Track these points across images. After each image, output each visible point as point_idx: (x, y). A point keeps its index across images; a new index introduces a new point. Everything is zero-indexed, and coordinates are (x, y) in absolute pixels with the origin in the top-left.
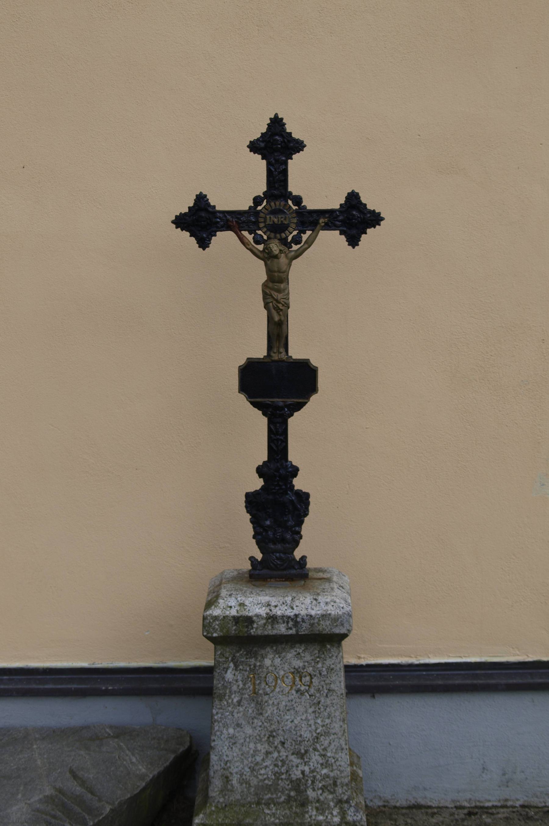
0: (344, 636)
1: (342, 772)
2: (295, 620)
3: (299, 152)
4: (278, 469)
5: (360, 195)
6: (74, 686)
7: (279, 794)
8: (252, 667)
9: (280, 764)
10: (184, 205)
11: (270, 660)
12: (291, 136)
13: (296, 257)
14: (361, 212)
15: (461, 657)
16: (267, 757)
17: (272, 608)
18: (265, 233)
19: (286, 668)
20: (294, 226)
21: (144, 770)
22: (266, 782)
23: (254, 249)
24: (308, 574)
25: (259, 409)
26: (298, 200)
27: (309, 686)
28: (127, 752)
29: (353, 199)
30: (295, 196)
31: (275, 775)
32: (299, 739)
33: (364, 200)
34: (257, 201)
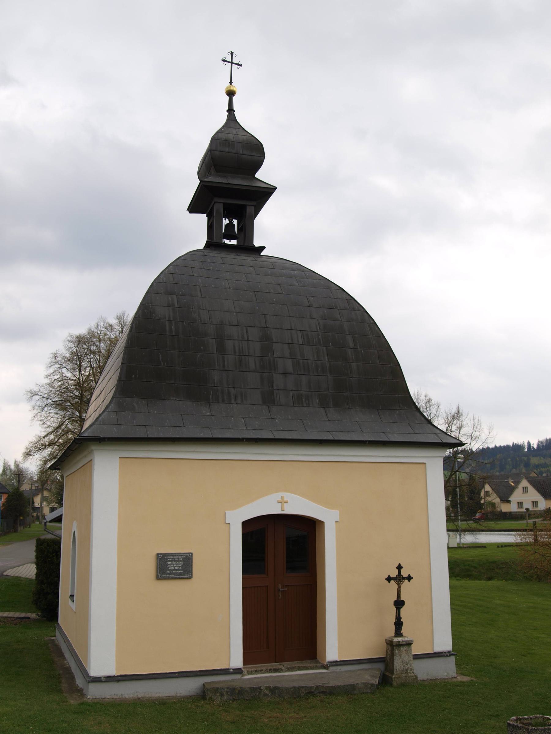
2: (406, 641)
11: (402, 649)
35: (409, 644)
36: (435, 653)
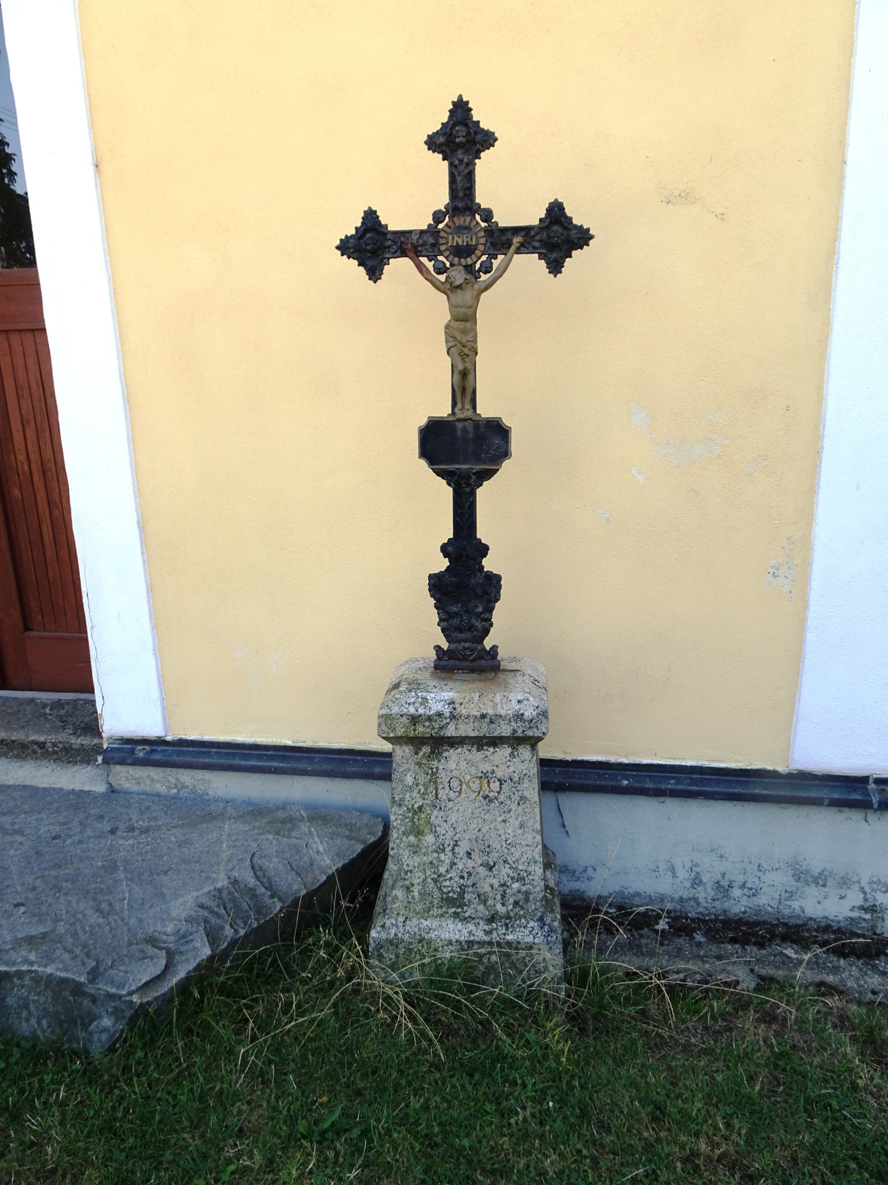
0: (540, 739)
1: (534, 887)
3: (488, 149)
4: (465, 547)
5: (565, 205)
6: (275, 764)
7: (465, 908)
8: (434, 770)
9: (466, 876)
10: (350, 224)
12: (479, 126)
13: (486, 288)
14: (566, 228)
15: (674, 758)
16: (451, 868)
17: (457, 706)
18: (447, 258)
19: (473, 773)
20: (481, 248)
21: (328, 862)
22: (451, 895)
23: (434, 280)
24: (499, 666)
25: (443, 478)
26: (487, 215)
27: (499, 793)
28: (316, 838)
29: (556, 213)
30: (484, 209)
31: (460, 887)
32: (487, 850)
33: (569, 212)
34: (438, 217)
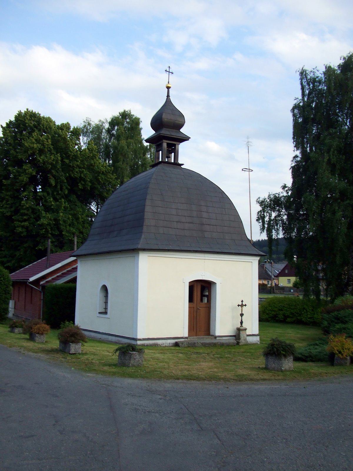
35: (246, 329)
36: (253, 335)
